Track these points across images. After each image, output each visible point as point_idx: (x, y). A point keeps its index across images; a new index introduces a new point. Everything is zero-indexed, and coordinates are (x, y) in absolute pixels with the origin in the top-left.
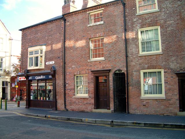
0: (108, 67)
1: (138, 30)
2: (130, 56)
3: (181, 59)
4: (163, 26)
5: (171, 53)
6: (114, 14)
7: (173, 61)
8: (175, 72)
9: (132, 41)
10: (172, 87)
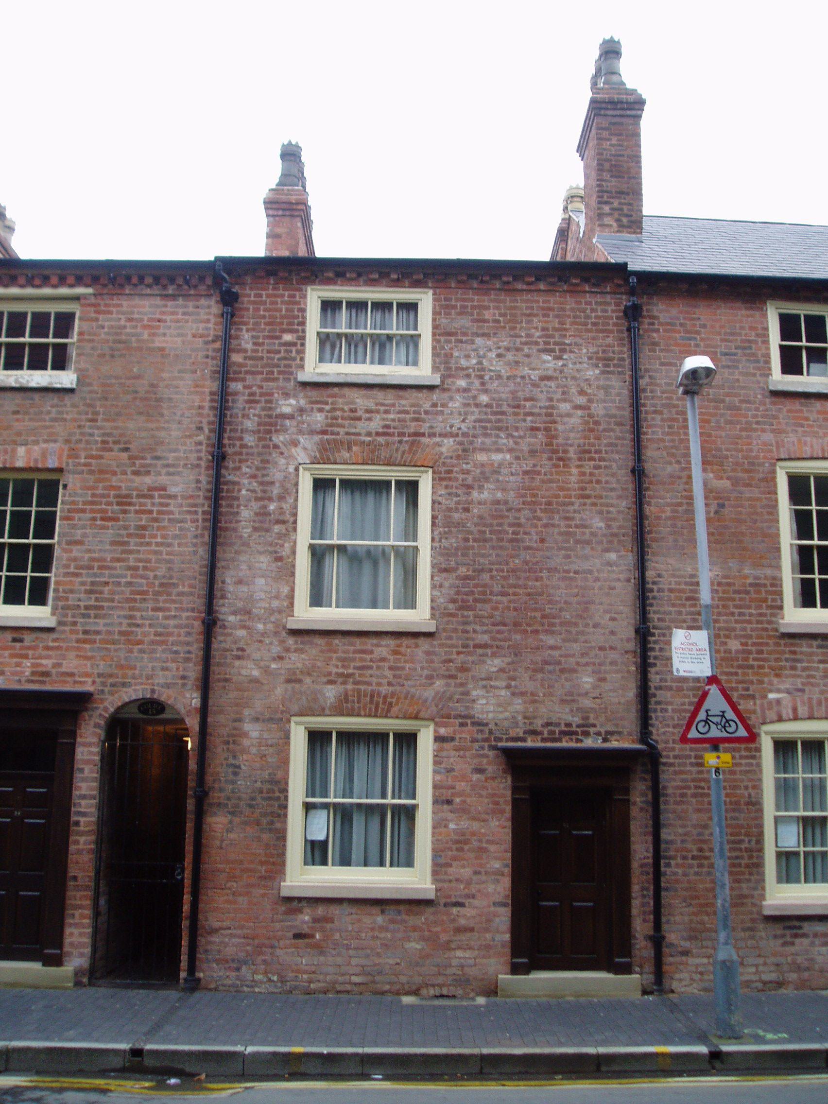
0: (72, 675)
1: (297, 469)
2: (232, 618)
3: (535, 670)
4: (449, 472)
5: (485, 632)
6: (158, 342)
7: (489, 679)
8: (500, 744)
9: (255, 529)
10: (476, 825)
